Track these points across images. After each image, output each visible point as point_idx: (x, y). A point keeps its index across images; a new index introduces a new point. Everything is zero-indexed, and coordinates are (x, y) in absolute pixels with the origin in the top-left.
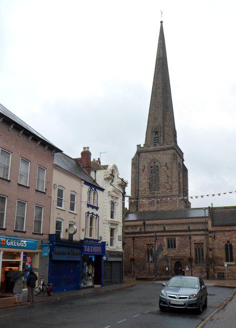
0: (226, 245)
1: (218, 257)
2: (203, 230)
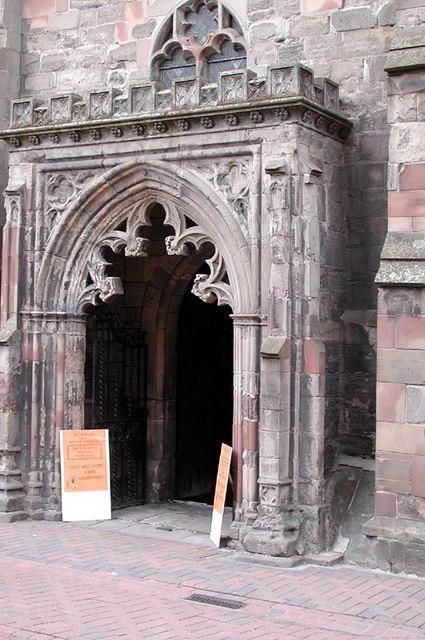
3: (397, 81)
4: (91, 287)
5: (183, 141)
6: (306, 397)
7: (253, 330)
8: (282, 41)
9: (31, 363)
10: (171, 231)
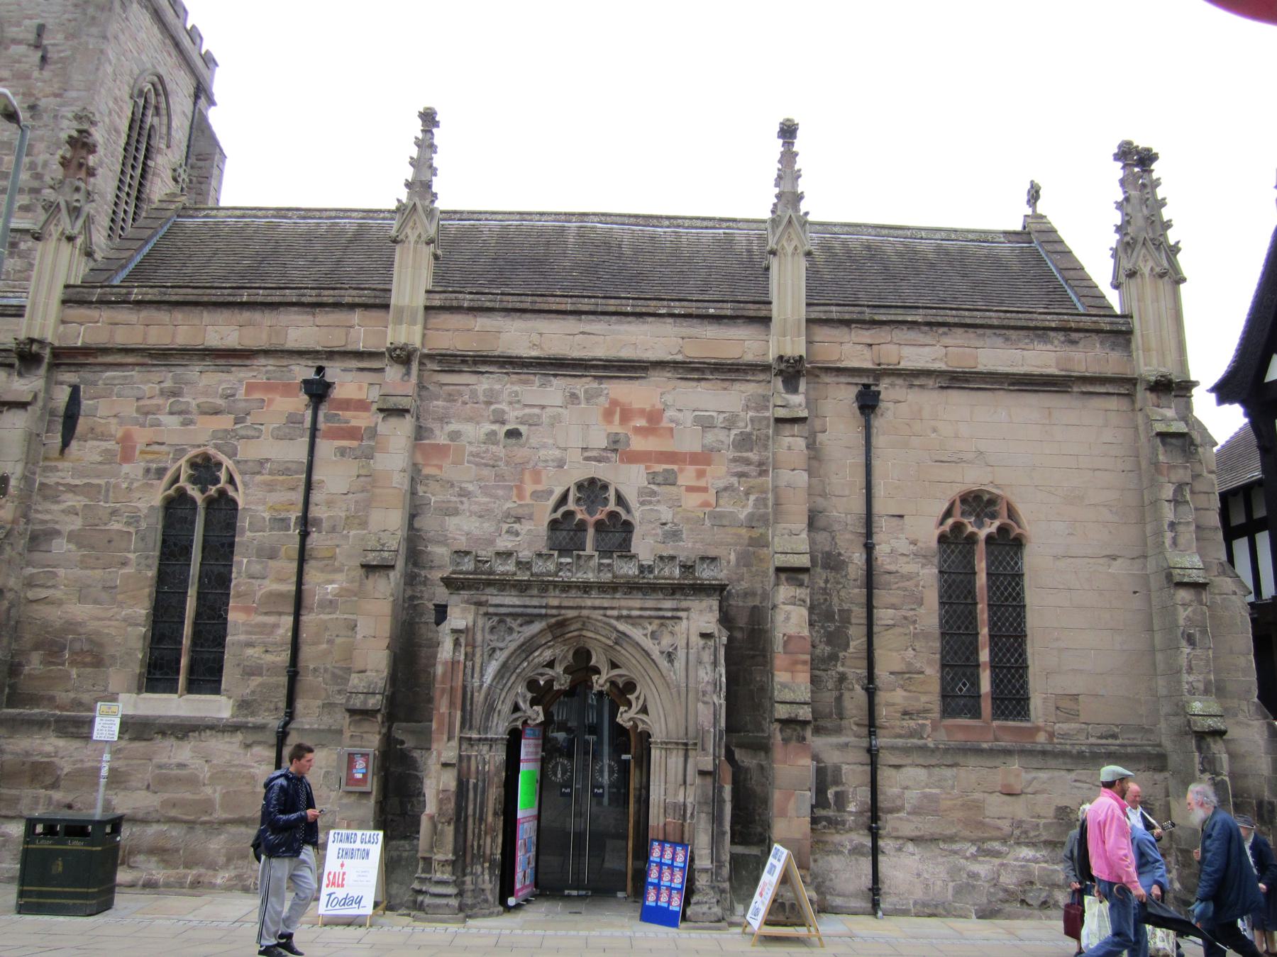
0: (176, 506)
3: (783, 576)
4: (518, 714)
5: (623, 603)
6: (721, 802)
7: (681, 753)
8: (664, 524)
9: (468, 781)
10: (597, 671)
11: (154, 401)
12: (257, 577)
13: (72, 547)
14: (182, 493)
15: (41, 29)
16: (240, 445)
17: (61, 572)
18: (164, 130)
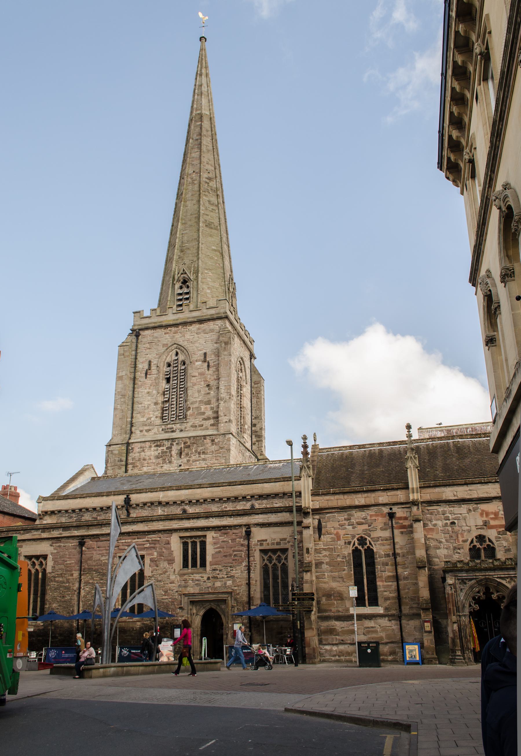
0: (356, 552)
1: (332, 589)
2: (289, 510)
11: (343, 522)
12: (384, 573)
13: (328, 566)
14: (356, 548)
15: (205, 354)
16: (372, 533)
17: (326, 574)
18: (244, 378)
